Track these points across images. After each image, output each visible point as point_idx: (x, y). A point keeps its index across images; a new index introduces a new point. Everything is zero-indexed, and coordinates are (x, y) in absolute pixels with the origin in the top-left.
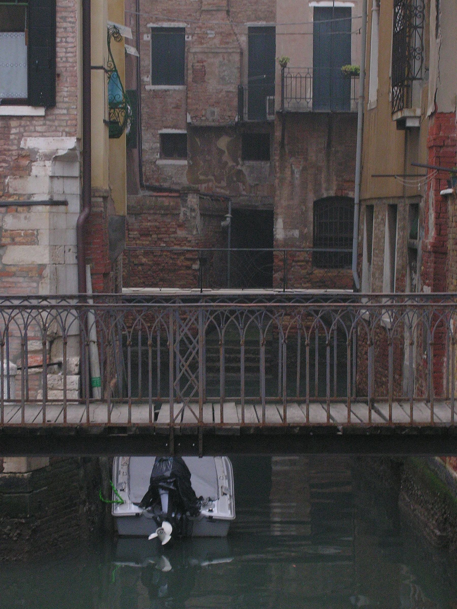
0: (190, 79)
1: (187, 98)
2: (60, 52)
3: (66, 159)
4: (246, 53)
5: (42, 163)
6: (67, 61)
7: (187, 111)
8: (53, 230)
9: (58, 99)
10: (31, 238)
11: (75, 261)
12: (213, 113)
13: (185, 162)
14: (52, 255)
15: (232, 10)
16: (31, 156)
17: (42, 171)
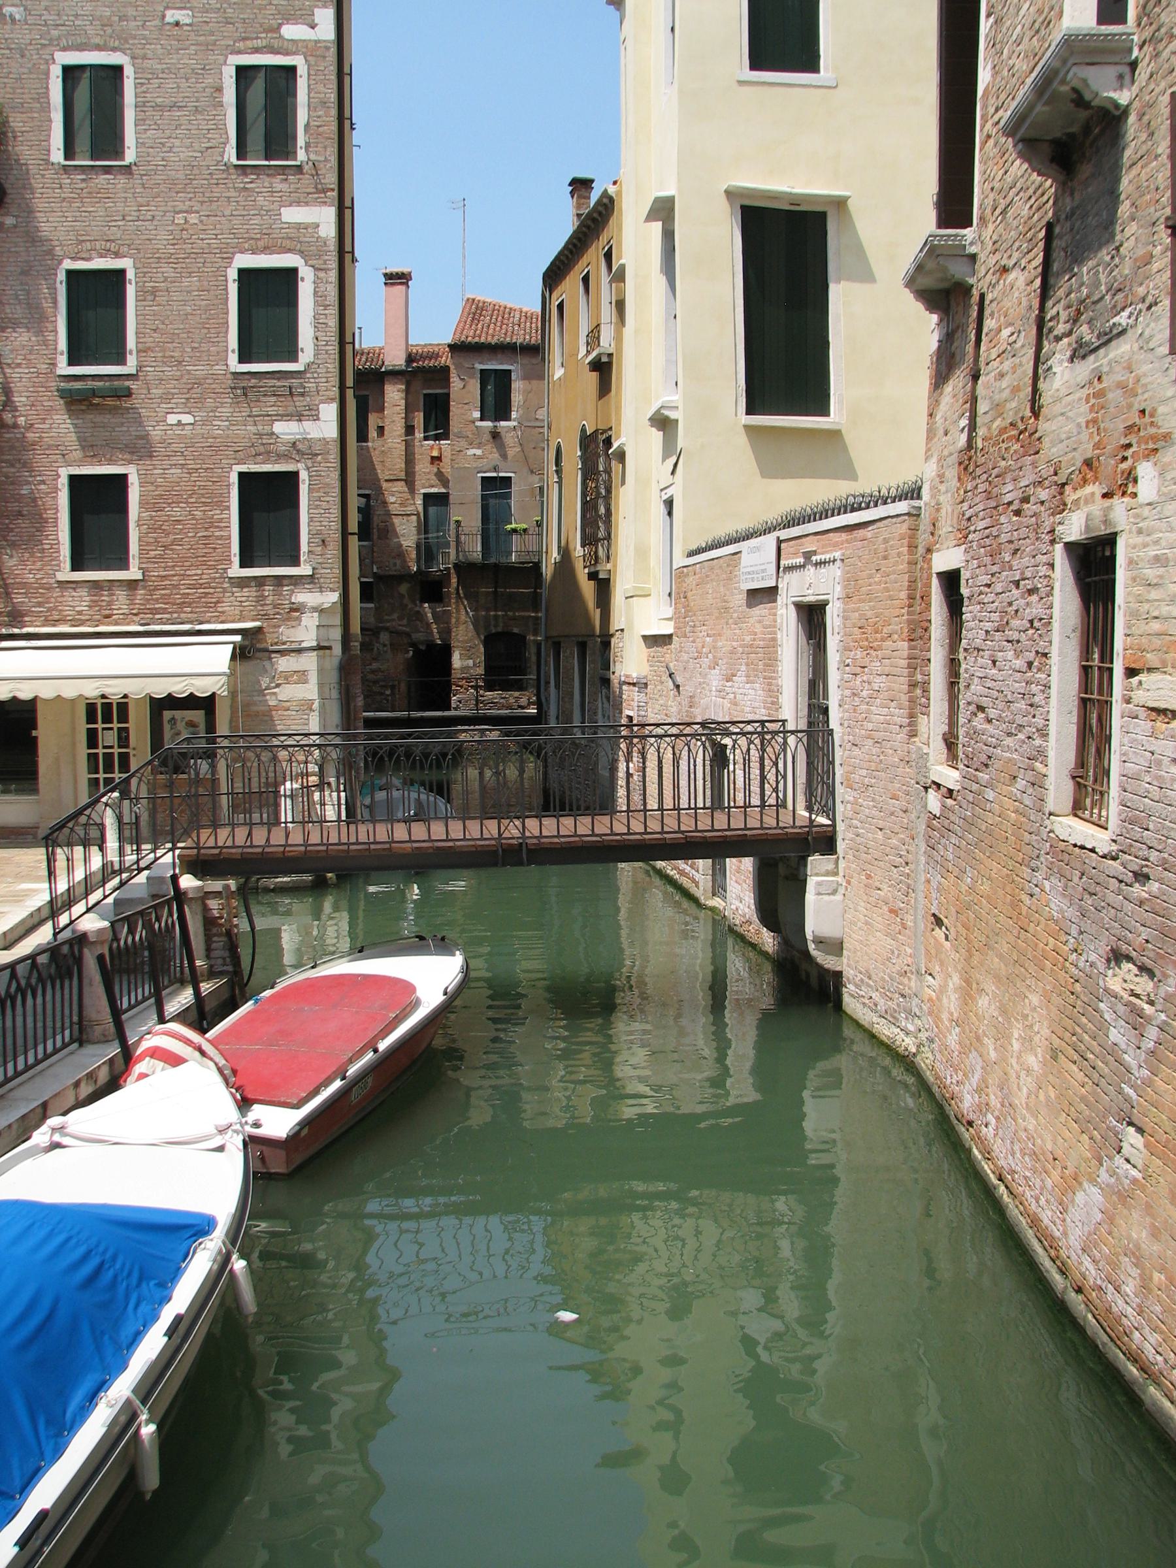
0: (375, 537)
8: (321, 671)
10: (301, 677)
12: (395, 564)
13: (372, 605)
16: (298, 609)
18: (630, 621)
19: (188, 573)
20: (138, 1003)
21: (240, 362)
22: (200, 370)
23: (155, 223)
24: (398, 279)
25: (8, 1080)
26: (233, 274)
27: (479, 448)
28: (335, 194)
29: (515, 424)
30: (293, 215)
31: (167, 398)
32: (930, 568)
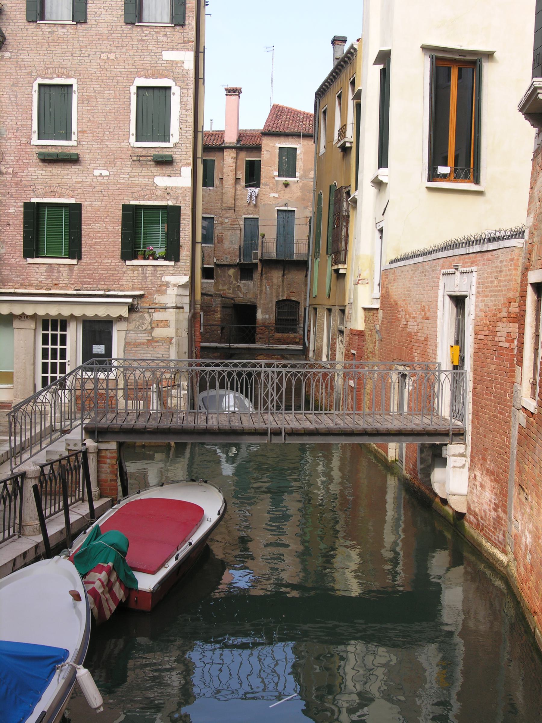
0: (216, 242)
1: (214, 250)
2: (182, 235)
3: (183, 286)
4: (243, 230)
5: (172, 288)
6: (185, 240)
7: (214, 257)
8: (177, 320)
9: (180, 257)
10: (165, 324)
11: (187, 336)
14: (176, 333)
15: (236, 209)
16: (167, 284)
17: (172, 292)
18: (356, 298)
19: (103, 261)
20: (55, 513)
21: (137, 141)
22: (113, 145)
23: (91, 58)
24: (234, 92)
25: (4, 540)
26: (134, 90)
27: (277, 193)
28: (194, 44)
29: (298, 179)
30: (169, 56)
31: (95, 159)
32: (527, 280)
